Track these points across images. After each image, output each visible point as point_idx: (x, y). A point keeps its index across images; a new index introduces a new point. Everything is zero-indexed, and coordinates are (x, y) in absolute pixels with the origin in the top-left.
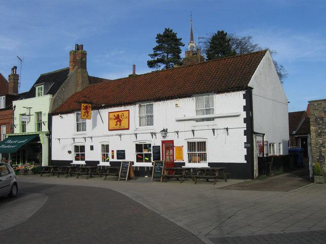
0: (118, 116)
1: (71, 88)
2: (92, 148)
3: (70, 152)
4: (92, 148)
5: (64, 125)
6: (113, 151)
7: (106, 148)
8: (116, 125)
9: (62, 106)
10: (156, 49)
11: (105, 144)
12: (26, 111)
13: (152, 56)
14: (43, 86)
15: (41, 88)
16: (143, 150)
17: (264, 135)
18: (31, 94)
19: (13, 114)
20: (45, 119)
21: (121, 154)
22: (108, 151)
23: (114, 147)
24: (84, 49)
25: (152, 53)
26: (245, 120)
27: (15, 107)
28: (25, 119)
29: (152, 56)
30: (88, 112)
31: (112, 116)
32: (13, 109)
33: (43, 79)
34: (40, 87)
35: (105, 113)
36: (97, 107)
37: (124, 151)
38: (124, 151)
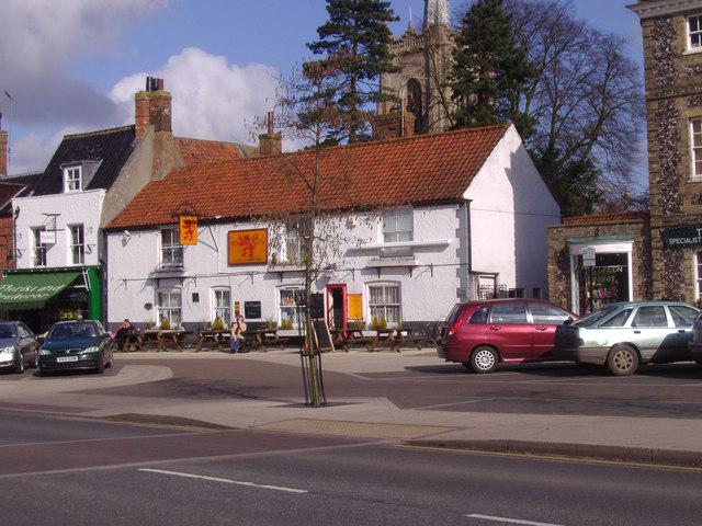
0: (247, 238)
1: (137, 175)
2: (196, 297)
3: (148, 306)
4: (196, 297)
5: (135, 257)
6: (237, 303)
7: (224, 295)
8: (244, 255)
9: (126, 211)
10: (323, 31)
11: (222, 289)
12: (46, 222)
13: (315, 48)
14: (80, 168)
15: (77, 172)
16: (262, 319)
17: (496, 275)
18: (47, 183)
19: (12, 226)
20: (91, 239)
21: (253, 309)
22: (228, 303)
23: (241, 296)
24: (167, 88)
25: (316, 38)
26: (459, 253)
27: (17, 212)
28: (46, 238)
29: (315, 48)
30: (191, 232)
31: (235, 237)
32: (11, 215)
33: (71, 151)
34: (73, 169)
35: (222, 232)
36: (207, 222)
37: (259, 303)
38: (259, 303)
